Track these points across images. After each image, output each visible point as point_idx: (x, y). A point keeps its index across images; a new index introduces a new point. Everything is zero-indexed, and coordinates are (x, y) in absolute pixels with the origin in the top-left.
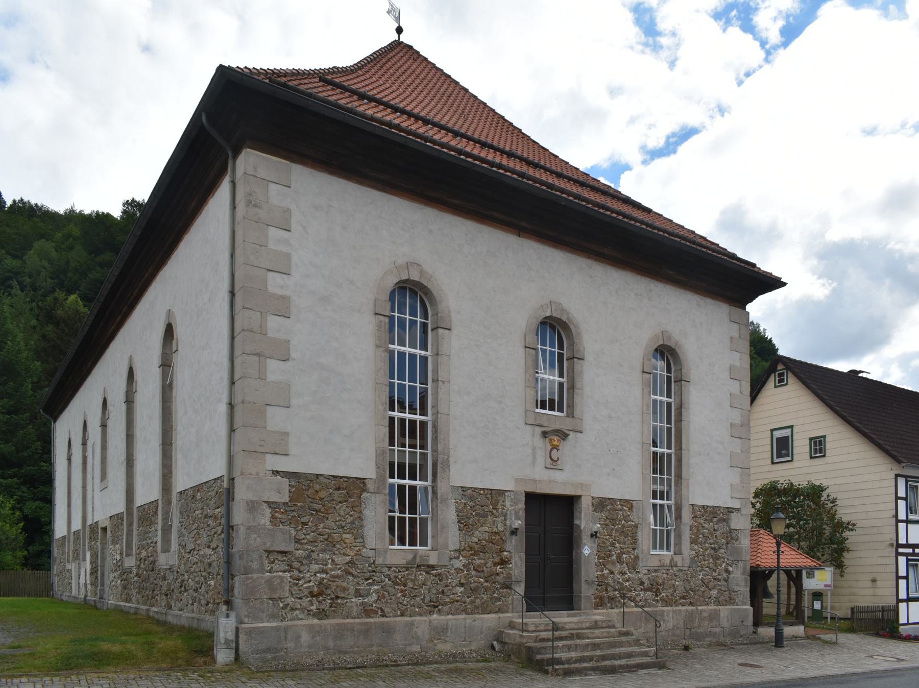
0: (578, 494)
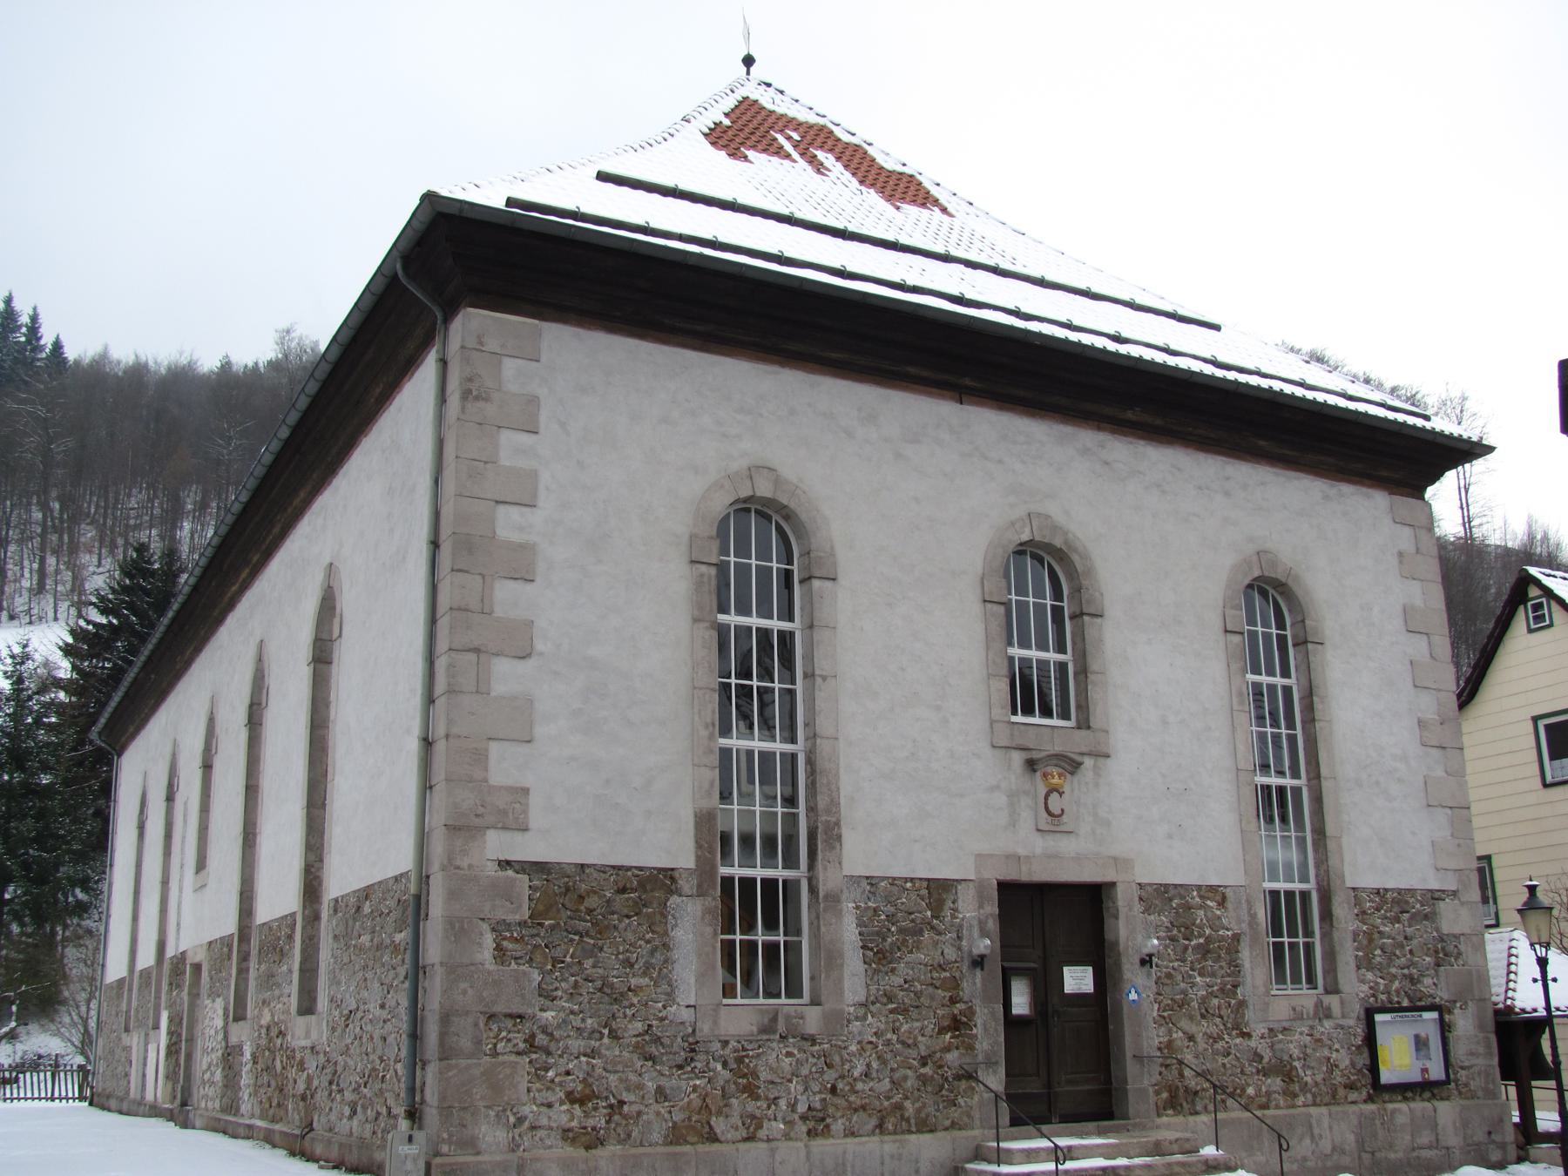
0: (1108, 878)
